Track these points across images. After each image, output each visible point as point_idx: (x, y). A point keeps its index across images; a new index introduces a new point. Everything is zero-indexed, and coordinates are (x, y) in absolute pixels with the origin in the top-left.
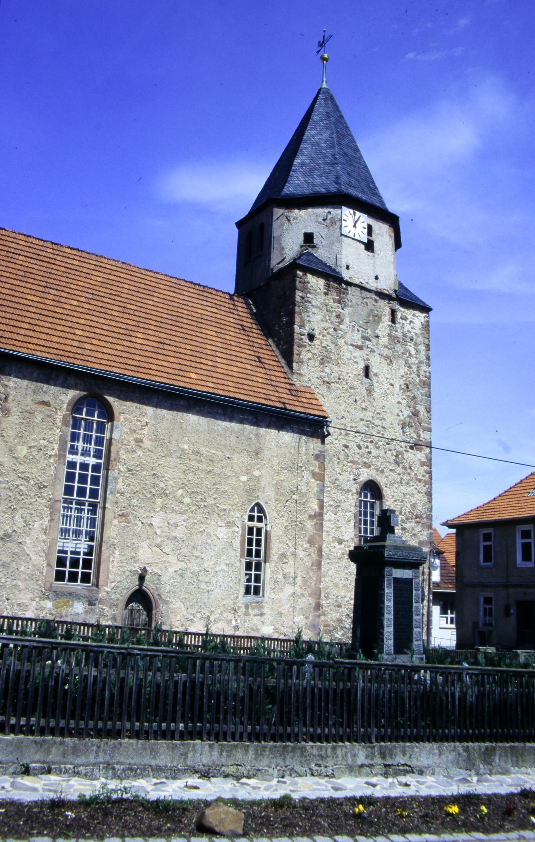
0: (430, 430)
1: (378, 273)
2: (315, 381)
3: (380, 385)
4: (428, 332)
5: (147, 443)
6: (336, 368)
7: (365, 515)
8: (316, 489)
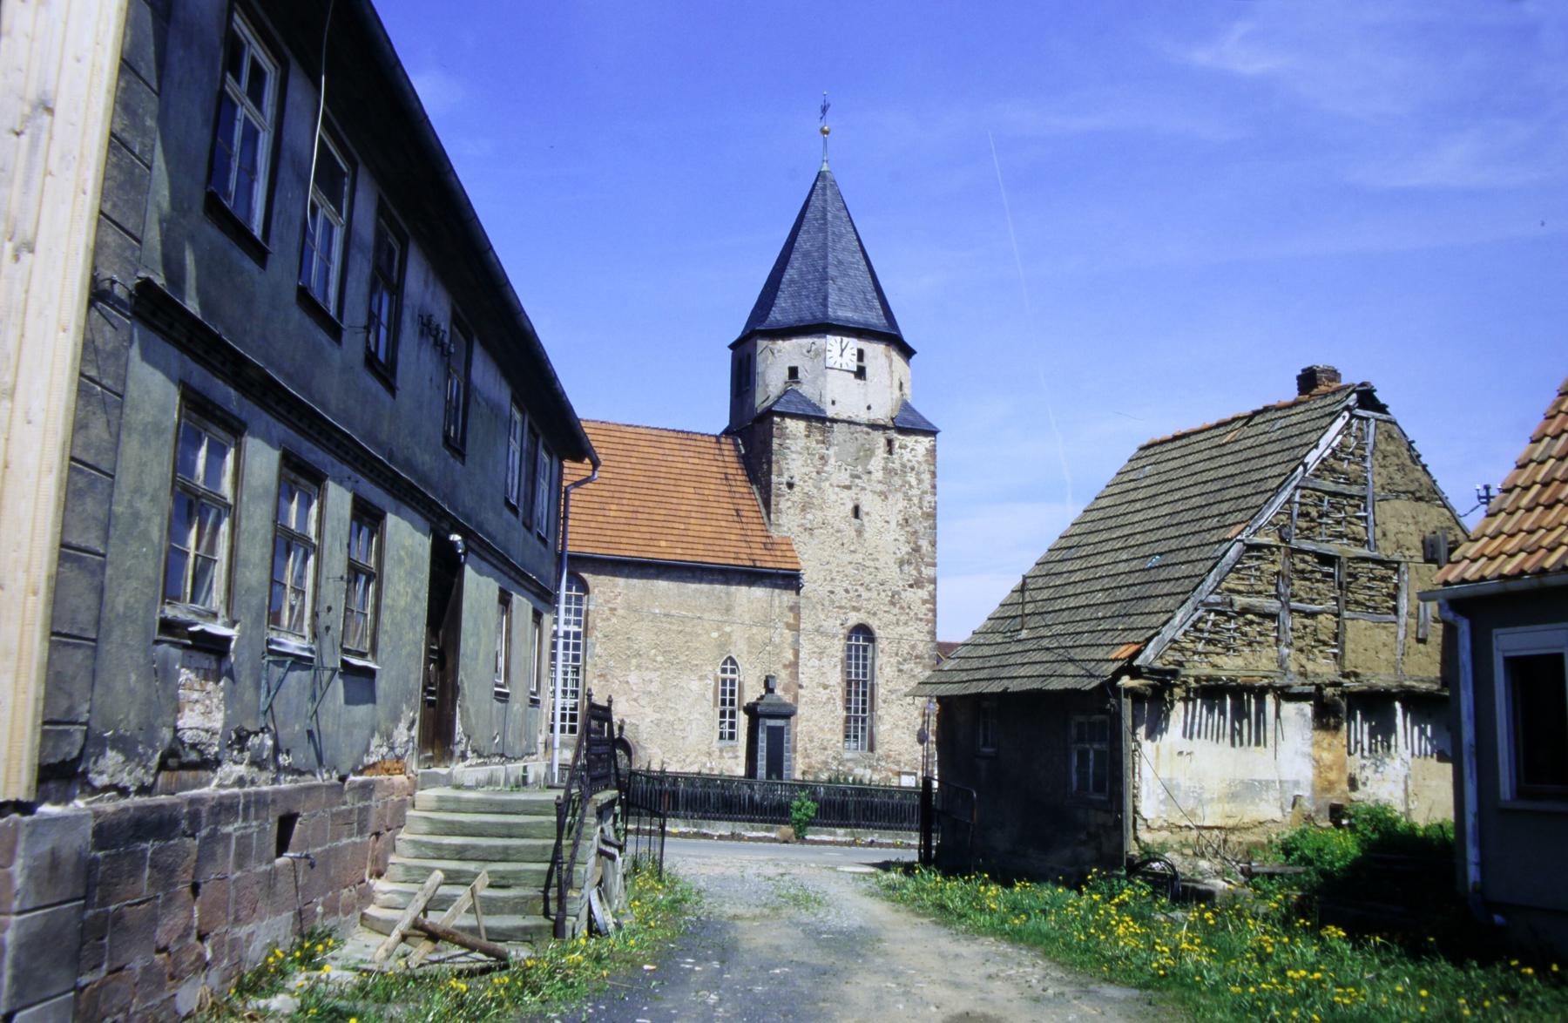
0: (934, 565)
1: (870, 402)
2: (796, 530)
3: (871, 523)
4: (934, 457)
5: (620, 612)
6: (819, 513)
7: (857, 658)
8: (790, 640)
